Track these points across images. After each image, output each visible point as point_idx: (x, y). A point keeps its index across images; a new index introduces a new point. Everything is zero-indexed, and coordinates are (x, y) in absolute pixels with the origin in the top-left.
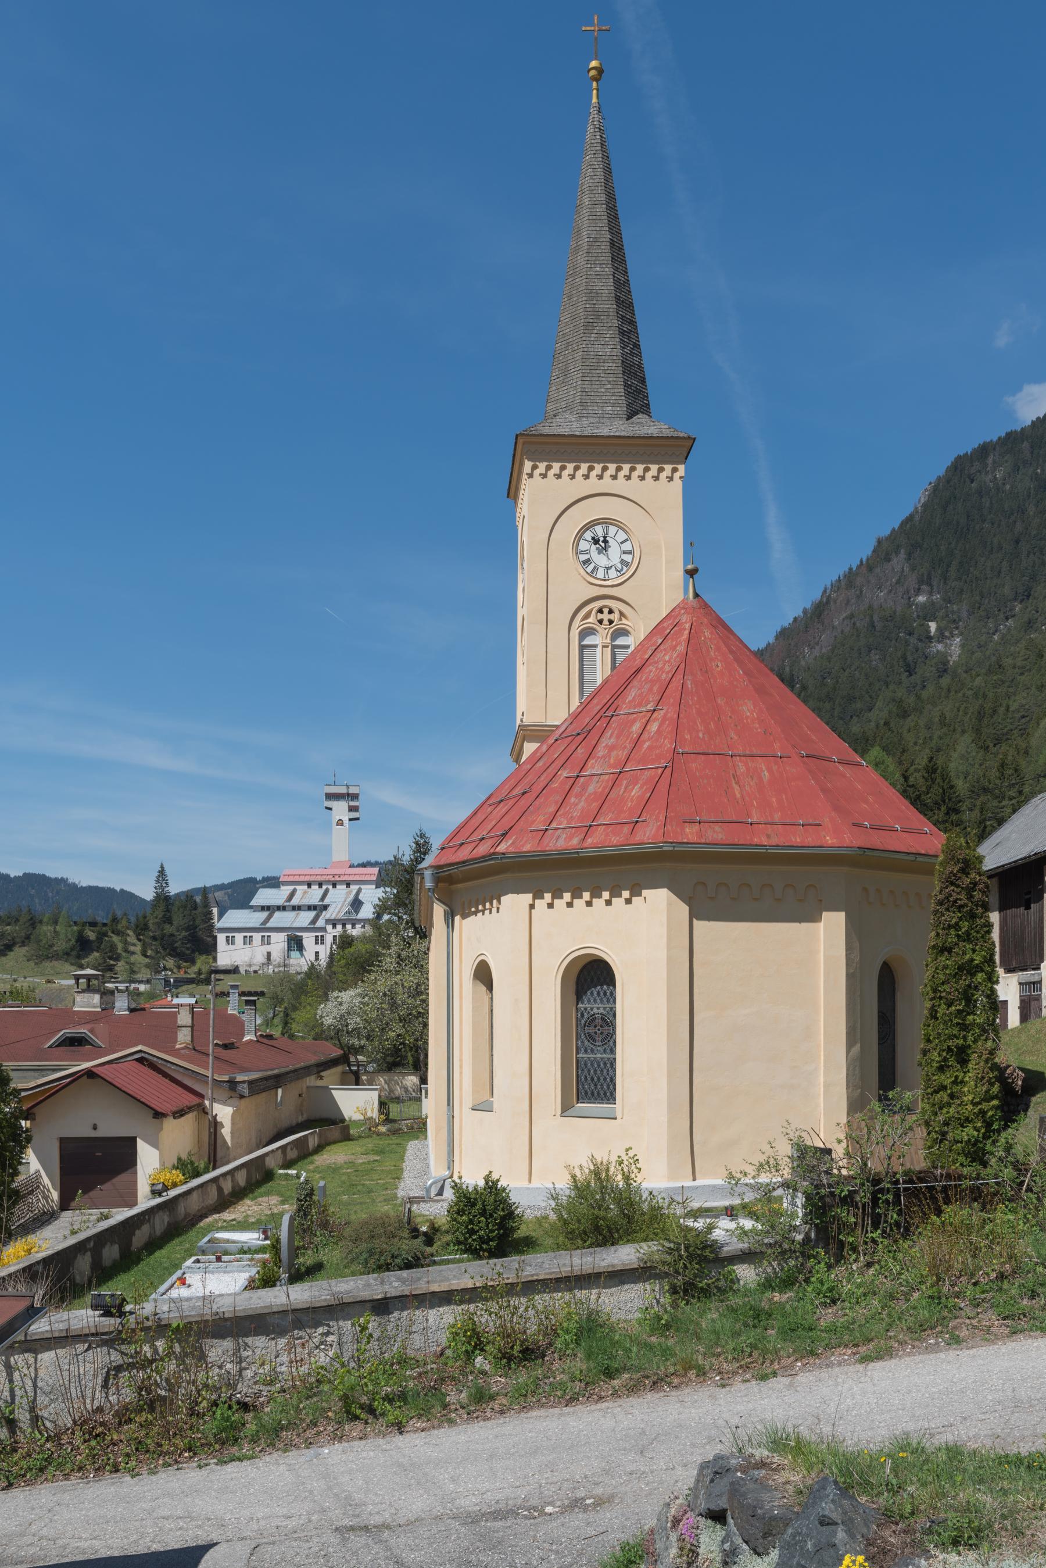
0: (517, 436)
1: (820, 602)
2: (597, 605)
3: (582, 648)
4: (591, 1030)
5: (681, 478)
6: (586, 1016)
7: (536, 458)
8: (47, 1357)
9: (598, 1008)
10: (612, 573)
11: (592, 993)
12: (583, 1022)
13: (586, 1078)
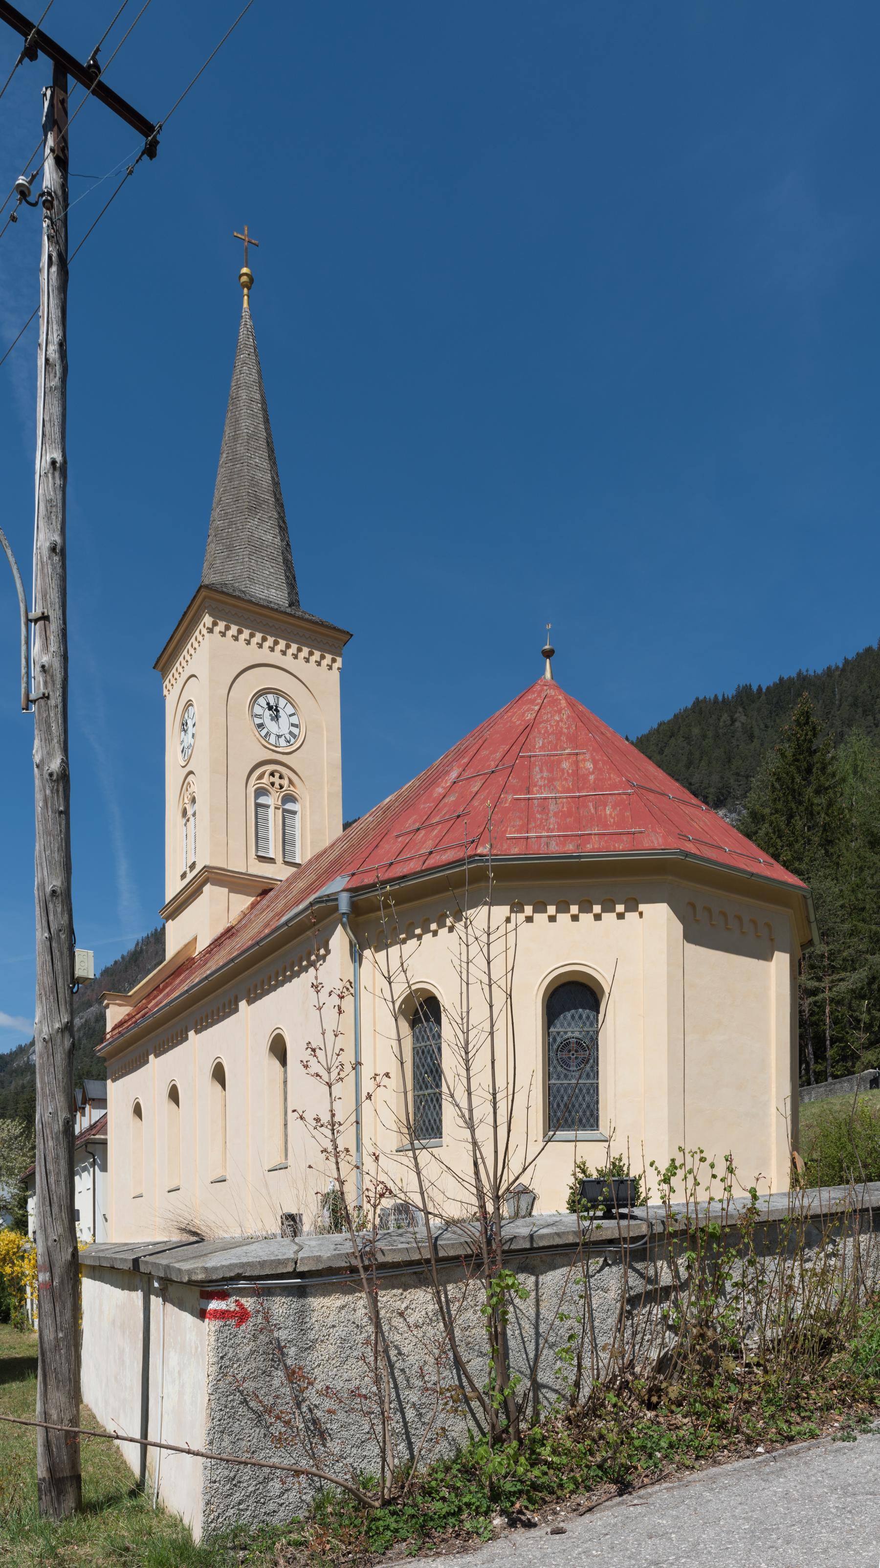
0: (201, 587)
1: (136, 950)
2: (270, 768)
3: (258, 805)
4: (565, 1055)
5: (339, 669)
6: (559, 1040)
7: (217, 616)
8: (552, 1279)
9: (572, 1032)
10: (282, 741)
11: (565, 1018)
12: (555, 1047)
13: (558, 1105)
